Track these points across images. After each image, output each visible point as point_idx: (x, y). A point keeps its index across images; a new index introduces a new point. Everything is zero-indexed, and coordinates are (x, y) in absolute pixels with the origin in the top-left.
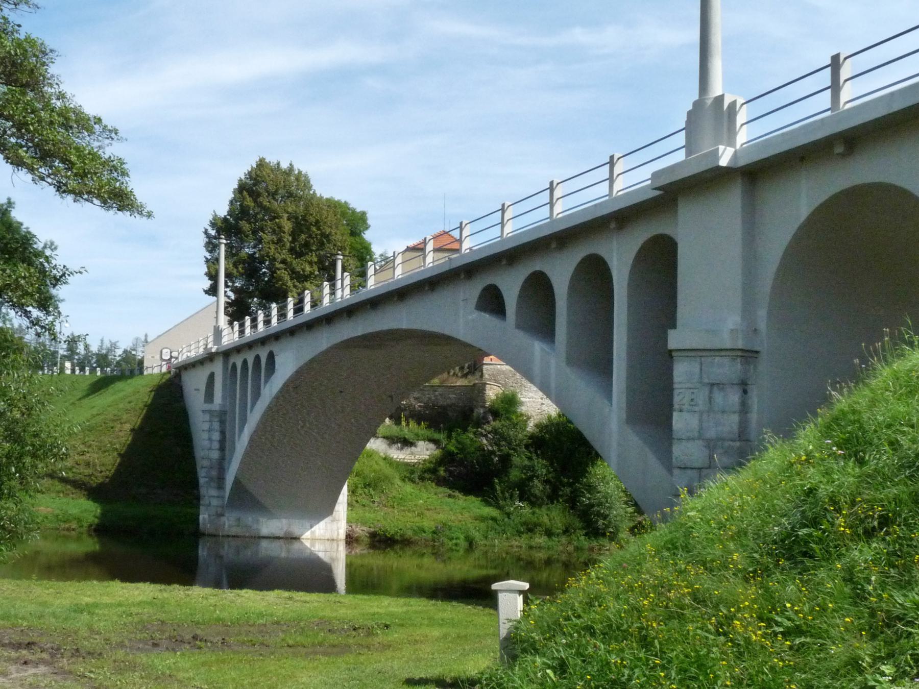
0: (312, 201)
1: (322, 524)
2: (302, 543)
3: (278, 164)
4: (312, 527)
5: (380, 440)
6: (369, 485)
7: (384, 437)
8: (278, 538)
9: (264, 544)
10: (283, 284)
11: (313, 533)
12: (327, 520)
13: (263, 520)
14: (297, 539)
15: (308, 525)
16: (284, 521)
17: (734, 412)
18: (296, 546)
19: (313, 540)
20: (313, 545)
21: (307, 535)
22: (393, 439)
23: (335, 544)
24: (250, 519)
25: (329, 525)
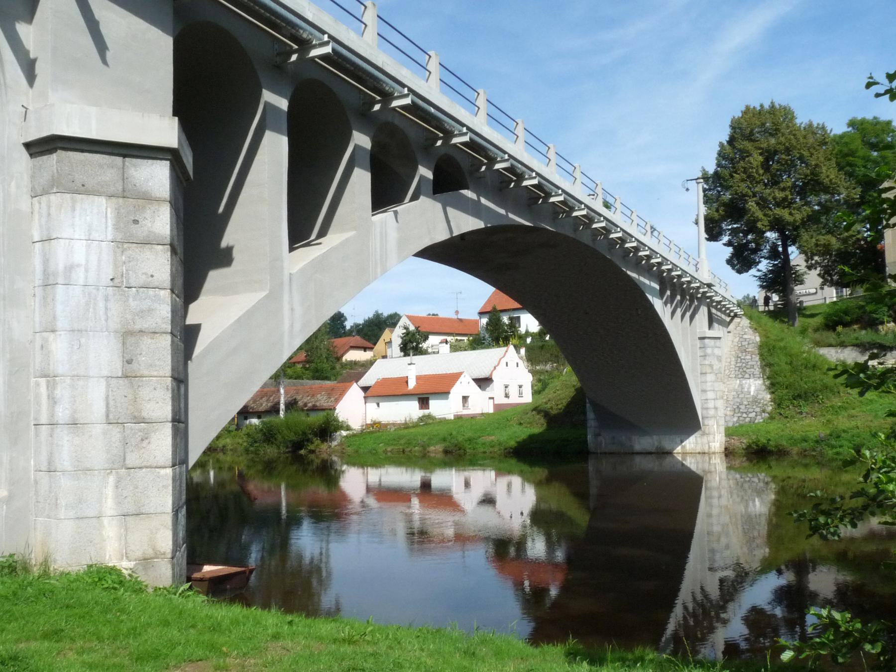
0: (794, 131)
1: (692, 439)
2: (674, 457)
3: (762, 106)
4: (682, 442)
5: (849, 348)
6: (799, 396)
7: (854, 345)
8: (650, 453)
9: (638, 459)
10: (752, 216)
11: (684, 447)
12: (697, 434)
13: (635, 438)
14: (670, 453)
15: (678, 440)
16: (655, 437)
17: (124, 163)
18: (668, 459)
19: (684, 454)
20: (685, 459)
21: (679, 449)
22: (865, 346)
23: (707, 458)
24: (624, 438)
25: (699, 439)
